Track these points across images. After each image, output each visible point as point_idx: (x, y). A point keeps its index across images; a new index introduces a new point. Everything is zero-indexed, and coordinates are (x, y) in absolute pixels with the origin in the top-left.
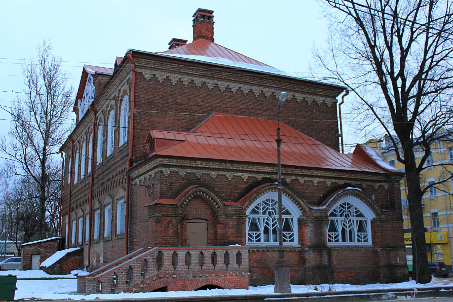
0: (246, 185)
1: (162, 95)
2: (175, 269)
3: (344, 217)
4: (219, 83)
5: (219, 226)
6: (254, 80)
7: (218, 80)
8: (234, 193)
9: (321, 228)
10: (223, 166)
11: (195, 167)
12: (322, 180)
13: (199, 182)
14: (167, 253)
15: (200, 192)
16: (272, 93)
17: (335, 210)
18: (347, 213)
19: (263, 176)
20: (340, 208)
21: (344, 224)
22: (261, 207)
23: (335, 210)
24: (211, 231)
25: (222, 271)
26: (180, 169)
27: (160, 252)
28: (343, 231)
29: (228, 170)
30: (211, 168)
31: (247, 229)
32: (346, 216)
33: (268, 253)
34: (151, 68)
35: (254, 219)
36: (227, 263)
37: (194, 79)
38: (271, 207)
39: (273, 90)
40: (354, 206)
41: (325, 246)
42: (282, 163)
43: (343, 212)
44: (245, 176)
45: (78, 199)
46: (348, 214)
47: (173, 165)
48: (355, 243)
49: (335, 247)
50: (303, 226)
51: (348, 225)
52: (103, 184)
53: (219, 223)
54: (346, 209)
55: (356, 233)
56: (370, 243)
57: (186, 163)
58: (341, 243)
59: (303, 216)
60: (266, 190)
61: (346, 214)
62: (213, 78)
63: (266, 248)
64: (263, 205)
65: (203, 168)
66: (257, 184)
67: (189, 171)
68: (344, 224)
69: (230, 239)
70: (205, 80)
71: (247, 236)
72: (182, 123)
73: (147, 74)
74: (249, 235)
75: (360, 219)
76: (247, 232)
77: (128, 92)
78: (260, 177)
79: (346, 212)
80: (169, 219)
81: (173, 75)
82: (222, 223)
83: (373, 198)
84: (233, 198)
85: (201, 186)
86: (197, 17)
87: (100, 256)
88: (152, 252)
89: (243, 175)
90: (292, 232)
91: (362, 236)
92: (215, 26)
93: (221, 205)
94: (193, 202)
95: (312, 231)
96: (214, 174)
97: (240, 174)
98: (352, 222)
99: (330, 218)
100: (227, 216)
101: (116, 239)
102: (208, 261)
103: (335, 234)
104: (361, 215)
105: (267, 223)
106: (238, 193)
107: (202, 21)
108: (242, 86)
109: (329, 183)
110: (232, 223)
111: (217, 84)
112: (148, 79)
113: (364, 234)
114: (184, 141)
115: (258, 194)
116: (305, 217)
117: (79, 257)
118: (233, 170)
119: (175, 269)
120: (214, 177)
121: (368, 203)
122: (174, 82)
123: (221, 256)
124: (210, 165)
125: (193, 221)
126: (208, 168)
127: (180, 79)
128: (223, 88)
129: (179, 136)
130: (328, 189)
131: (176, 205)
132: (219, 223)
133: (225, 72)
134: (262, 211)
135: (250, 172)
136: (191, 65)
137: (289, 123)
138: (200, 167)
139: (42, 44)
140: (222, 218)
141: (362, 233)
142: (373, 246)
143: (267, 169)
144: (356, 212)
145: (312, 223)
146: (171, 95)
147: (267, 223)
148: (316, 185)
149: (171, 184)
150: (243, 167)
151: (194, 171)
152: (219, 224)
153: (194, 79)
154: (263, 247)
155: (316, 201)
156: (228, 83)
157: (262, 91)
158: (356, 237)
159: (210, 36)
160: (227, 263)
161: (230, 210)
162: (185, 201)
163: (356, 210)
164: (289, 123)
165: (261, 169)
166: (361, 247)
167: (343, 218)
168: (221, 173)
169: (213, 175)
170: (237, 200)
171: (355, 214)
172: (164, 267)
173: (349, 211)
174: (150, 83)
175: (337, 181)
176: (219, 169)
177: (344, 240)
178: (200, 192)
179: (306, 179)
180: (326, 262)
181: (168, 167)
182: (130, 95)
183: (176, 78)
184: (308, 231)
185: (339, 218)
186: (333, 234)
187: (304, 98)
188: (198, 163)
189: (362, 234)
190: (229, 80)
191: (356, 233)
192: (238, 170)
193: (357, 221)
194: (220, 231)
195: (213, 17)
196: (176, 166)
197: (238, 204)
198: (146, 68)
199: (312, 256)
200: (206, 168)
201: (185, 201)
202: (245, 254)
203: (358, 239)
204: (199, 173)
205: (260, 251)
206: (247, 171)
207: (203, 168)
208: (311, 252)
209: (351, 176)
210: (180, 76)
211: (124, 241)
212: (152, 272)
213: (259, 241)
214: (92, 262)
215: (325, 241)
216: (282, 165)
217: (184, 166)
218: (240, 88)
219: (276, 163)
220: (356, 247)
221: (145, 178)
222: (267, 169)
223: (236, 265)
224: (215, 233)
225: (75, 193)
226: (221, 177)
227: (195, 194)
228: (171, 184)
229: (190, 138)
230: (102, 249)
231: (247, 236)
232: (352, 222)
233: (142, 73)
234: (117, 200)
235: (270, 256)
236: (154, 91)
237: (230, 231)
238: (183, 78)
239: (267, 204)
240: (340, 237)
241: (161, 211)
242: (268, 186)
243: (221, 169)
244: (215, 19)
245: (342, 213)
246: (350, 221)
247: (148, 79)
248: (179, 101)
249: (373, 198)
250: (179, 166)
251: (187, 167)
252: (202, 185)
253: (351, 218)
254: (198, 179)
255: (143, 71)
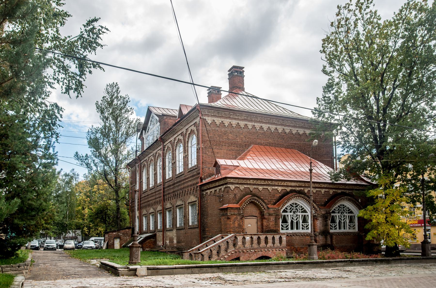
0: (280, 195)
1: (219, 134)
2: (244, 247)
3: (340, 214)
4: (256, 124)
5: (264, 220)
6: (278, 122)
7: (255, 123)
8: (273, 199)
9: (326, 221)
10: (266, 182)
11: (249, 184)
12: (327, 190)
13: (251, 193)
14: (270, 237)
15: (253, 199)
16: (290, 130)
17: (335, 209)
18: (295, 210)
19: (290, 188)
20: (290, 207)
21: (340, 218)
22: (289, 208)
23: (335, 209)
24: (259, 224)
25: (264, 248)
26: (241, 186)
27: (236, 237)
28: (292, 222)
29: (269, 185)
30: (259, 184)
31: (281, 221)
32: (294, 212)
33: (294, 237)
34: (211, 115)
35: (284, 216)
36: (274, 243)
37: (239, 122)
38: (295, 208)
39: (291, 128)
40: (347, 207)
41: (329, 233)
42: (313, 180)
43: (292, 209)
44: (280, 189)
45: (149, 201)
46: (343, 212)
47: (236, 183)
48: (301, 231)
49: (334, 233)
50: (315, 220)
51: (343, 219)
52: (174, 192)
53: (265, 219)
54: (341, 208)
55: (301, 224)
56: (357, 230)
57: (244, 181)
58: (338, 231)
59: (315, 213)
60: (293, 198)
61: (294, 211)
62: (251, 121)
63: (292, 233)
64: (290, 207)
65: (254, 184)
66: (287, 193)
67: (246, 186)
68: (340, 218)
69: (271, 228)
70: (246, 123)
71: (281, 227)
72: (232, 152)
73: (209, 120)
74: (282, 225)
75: (350, 215)
76: (281, 224)
77: (196, 132)
78: (289, 189)
79: (341, 210)
80: (235, 216)
81: (226, 120)
82: (266, 219)
83: (360, 201)
84: (272, 202)
85: (254, 196)
86: (232, 72)
87: (173, 239)
88: (231, 237)
89: (278, 188)
90: (308, 224)
91: (352, 226)
92: (245, 78)
93: (266, 208)
94: (248, 206)
95: (321, 223)
96: (261, 188)
97: (276, 188)
98: (298, 216)
99: (332, 214)
100: (270, 215)
101: (189, 228)
102: (255, 242)
103: (286, 225)
104: (351, 212)
105: (292, 218)
106: (275, 199)
107: (236, 75)
108: (270, 126)
109: (331, 192)
110: (272, 218)
111: (254, 125)
112: (210, 124)
113: (306, 224)
114: (239, 166)
115: (288, 200)
116: (316, 214)
117: (153, 240)
118: (272, 185)
119: (244, 247)
120: (261, 190)
121: (356, 204)
122: (226, 125)
123: (270, 239)
124: (259, 182)
125: (248, 217)
126: (257, 184)
127: (230, 122)
128: (258, 128)
129: (235, 162)
130: (330, 196)
131: (239, 208)
132: (265, 219)
133: (260, 116)
134: (289, 211)
135: (282, 186)
136: (238, 112)
137: (301, 150)
138: (252, 184)
139: (81, 92)
140: (266, 216)
141: (305, 224)
142: (359, 232)
143: (293, 184)
144: (348, 211)
145: (321, 218)
146: (225, 134)
147: (292, 218)
148: (323, 193)
149: (235, 195)
150: (278, 183)
151: (249, 186)
152: (265, 219)
153: (239, 122)
154: (291, 233)
155: (323, 203)
156: (261, 125)
157: (283, 129)
158: (301, 226)
159: (242, 86)
160: (274, 243)
161: (271, 211)
162: (245, 205)
163: (301, 207)
164: (301, 150)
165: (289, 184)
166: (351, 233)
167: (292, 213)
168: (265, 187)
169: (260, 189)
170: (275, 204)
171: (347, 212)
172: (238, 245)
173: (343, 210)
174: (212, 126)
175: (336, 191)
176: (263, 184)
177: (292, 228)
178: (253, 199)
179: (317, 189)
180: (329, 242)
181: (233, 184)
182: (198, 134)
183: (227, 122)
184: (319, 223)
185: (337, 215)
186: (333, 225)
187: (283, 129)
188: (251, 182)
189: (305, 225)
190: (261, 122)
191: (301, 224)
192: (275, 185)
193: (302, 216)
194: (265, 224)
195: (244, 71)
196: (238, 183)
197: (275, 206)
198: (208, 116)
199: (321, 238)
200: (256, 184)
201: (245, 205)
202: (284, 238)
203: (302, 228)
204: (252, 188)
205: (289, 235)
206: (281, 185)
207: (254, 184)
208: (320, 236)
209: (345, 187)
210: (230, 121)
211: (198, 230)
212: (231, 249)
213: (287, 229)
214: (166, 243)
215: (328, 229)
216: (313, 182)
217: (243, 183)
218: (269, 127)
219: (309, 180)
220: (348, 232)
221: (216, 191)
222: (293, 184)
223: (279, 244)
224: (262, 224)
225: (145, 197)
226: (265, 190)
227: (250, 201)
228: (235, 195)
229: (242, 163)
230: (175, 234)
231: (281, 227)
232: (298, 216)
233: (206, 119)
234: (188, 203)
235: (295, 239)
236: (214, 131)
237: (271, 224)
238: (232, 122)
239: (292, 206)
240: (289, 226)
241: (230, 212)
242: (294, 195)
243: (265, 184)
244: (245, 74)
245: (291, 210)
246: (297, 215)
247: (210, 124)
248: (230, 138)
249: (360, 201)
250: (239, 183)
251: (244, 183)
252: (254, 195)
253: (298, 214)
254: (251, 191)
255: (206, 118)
